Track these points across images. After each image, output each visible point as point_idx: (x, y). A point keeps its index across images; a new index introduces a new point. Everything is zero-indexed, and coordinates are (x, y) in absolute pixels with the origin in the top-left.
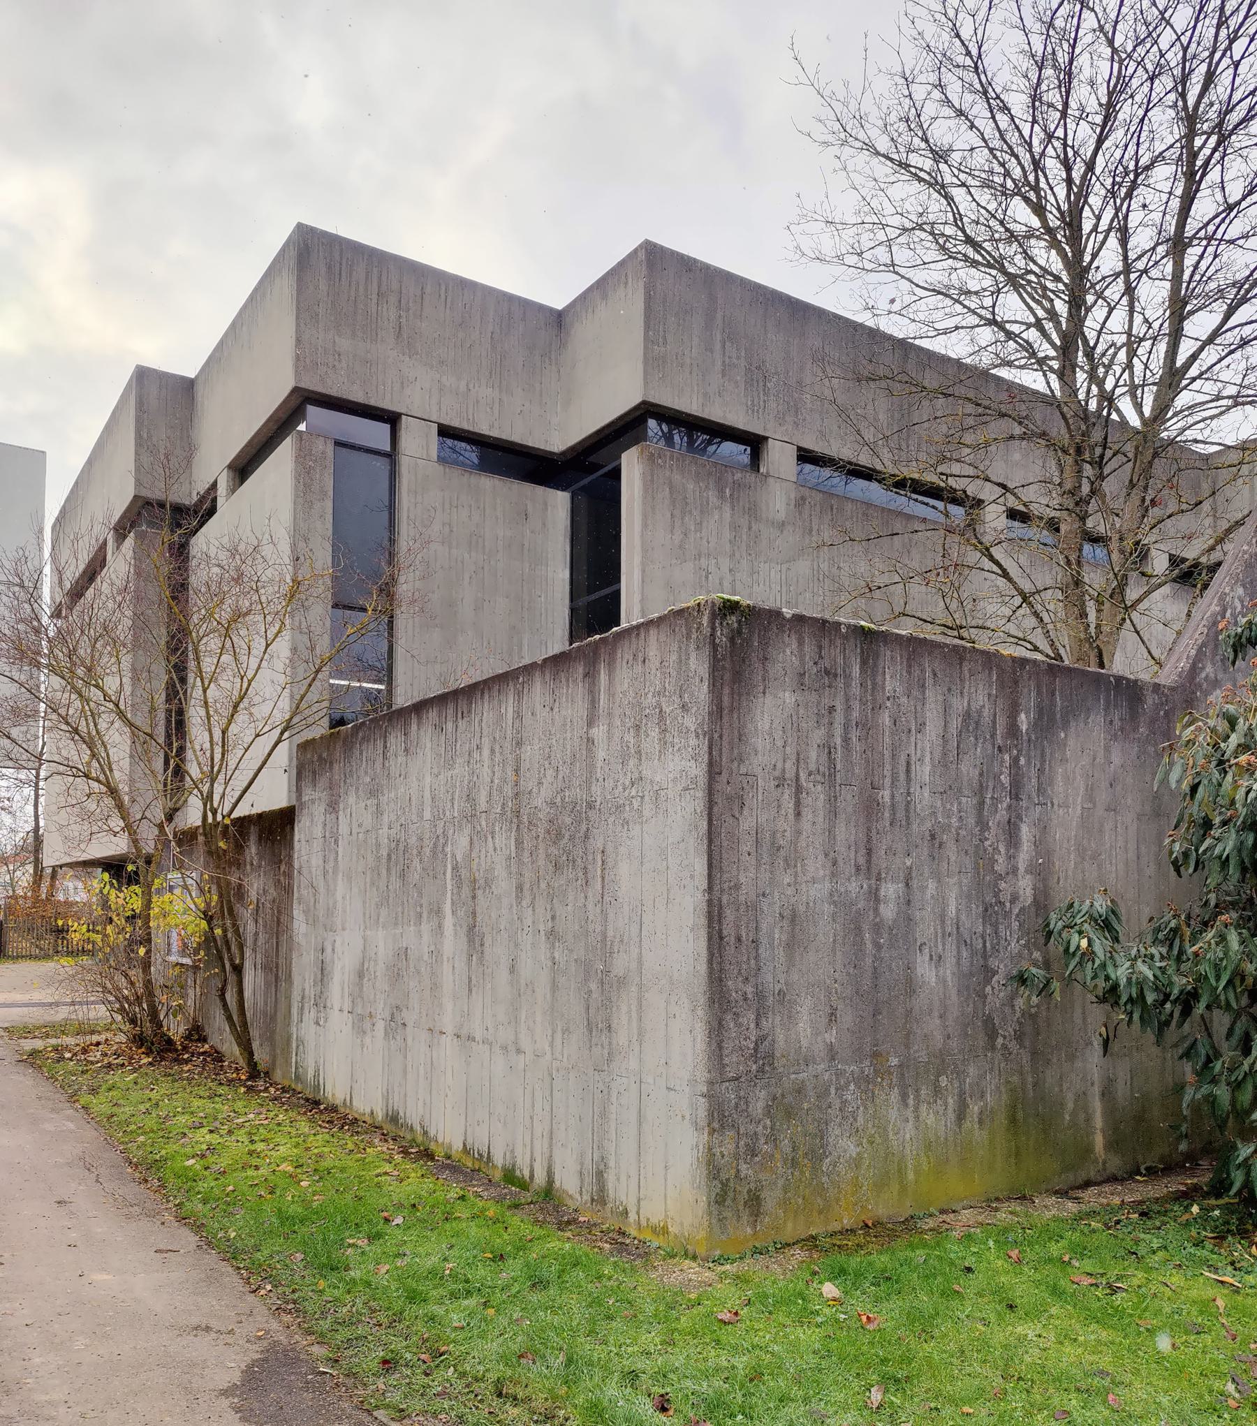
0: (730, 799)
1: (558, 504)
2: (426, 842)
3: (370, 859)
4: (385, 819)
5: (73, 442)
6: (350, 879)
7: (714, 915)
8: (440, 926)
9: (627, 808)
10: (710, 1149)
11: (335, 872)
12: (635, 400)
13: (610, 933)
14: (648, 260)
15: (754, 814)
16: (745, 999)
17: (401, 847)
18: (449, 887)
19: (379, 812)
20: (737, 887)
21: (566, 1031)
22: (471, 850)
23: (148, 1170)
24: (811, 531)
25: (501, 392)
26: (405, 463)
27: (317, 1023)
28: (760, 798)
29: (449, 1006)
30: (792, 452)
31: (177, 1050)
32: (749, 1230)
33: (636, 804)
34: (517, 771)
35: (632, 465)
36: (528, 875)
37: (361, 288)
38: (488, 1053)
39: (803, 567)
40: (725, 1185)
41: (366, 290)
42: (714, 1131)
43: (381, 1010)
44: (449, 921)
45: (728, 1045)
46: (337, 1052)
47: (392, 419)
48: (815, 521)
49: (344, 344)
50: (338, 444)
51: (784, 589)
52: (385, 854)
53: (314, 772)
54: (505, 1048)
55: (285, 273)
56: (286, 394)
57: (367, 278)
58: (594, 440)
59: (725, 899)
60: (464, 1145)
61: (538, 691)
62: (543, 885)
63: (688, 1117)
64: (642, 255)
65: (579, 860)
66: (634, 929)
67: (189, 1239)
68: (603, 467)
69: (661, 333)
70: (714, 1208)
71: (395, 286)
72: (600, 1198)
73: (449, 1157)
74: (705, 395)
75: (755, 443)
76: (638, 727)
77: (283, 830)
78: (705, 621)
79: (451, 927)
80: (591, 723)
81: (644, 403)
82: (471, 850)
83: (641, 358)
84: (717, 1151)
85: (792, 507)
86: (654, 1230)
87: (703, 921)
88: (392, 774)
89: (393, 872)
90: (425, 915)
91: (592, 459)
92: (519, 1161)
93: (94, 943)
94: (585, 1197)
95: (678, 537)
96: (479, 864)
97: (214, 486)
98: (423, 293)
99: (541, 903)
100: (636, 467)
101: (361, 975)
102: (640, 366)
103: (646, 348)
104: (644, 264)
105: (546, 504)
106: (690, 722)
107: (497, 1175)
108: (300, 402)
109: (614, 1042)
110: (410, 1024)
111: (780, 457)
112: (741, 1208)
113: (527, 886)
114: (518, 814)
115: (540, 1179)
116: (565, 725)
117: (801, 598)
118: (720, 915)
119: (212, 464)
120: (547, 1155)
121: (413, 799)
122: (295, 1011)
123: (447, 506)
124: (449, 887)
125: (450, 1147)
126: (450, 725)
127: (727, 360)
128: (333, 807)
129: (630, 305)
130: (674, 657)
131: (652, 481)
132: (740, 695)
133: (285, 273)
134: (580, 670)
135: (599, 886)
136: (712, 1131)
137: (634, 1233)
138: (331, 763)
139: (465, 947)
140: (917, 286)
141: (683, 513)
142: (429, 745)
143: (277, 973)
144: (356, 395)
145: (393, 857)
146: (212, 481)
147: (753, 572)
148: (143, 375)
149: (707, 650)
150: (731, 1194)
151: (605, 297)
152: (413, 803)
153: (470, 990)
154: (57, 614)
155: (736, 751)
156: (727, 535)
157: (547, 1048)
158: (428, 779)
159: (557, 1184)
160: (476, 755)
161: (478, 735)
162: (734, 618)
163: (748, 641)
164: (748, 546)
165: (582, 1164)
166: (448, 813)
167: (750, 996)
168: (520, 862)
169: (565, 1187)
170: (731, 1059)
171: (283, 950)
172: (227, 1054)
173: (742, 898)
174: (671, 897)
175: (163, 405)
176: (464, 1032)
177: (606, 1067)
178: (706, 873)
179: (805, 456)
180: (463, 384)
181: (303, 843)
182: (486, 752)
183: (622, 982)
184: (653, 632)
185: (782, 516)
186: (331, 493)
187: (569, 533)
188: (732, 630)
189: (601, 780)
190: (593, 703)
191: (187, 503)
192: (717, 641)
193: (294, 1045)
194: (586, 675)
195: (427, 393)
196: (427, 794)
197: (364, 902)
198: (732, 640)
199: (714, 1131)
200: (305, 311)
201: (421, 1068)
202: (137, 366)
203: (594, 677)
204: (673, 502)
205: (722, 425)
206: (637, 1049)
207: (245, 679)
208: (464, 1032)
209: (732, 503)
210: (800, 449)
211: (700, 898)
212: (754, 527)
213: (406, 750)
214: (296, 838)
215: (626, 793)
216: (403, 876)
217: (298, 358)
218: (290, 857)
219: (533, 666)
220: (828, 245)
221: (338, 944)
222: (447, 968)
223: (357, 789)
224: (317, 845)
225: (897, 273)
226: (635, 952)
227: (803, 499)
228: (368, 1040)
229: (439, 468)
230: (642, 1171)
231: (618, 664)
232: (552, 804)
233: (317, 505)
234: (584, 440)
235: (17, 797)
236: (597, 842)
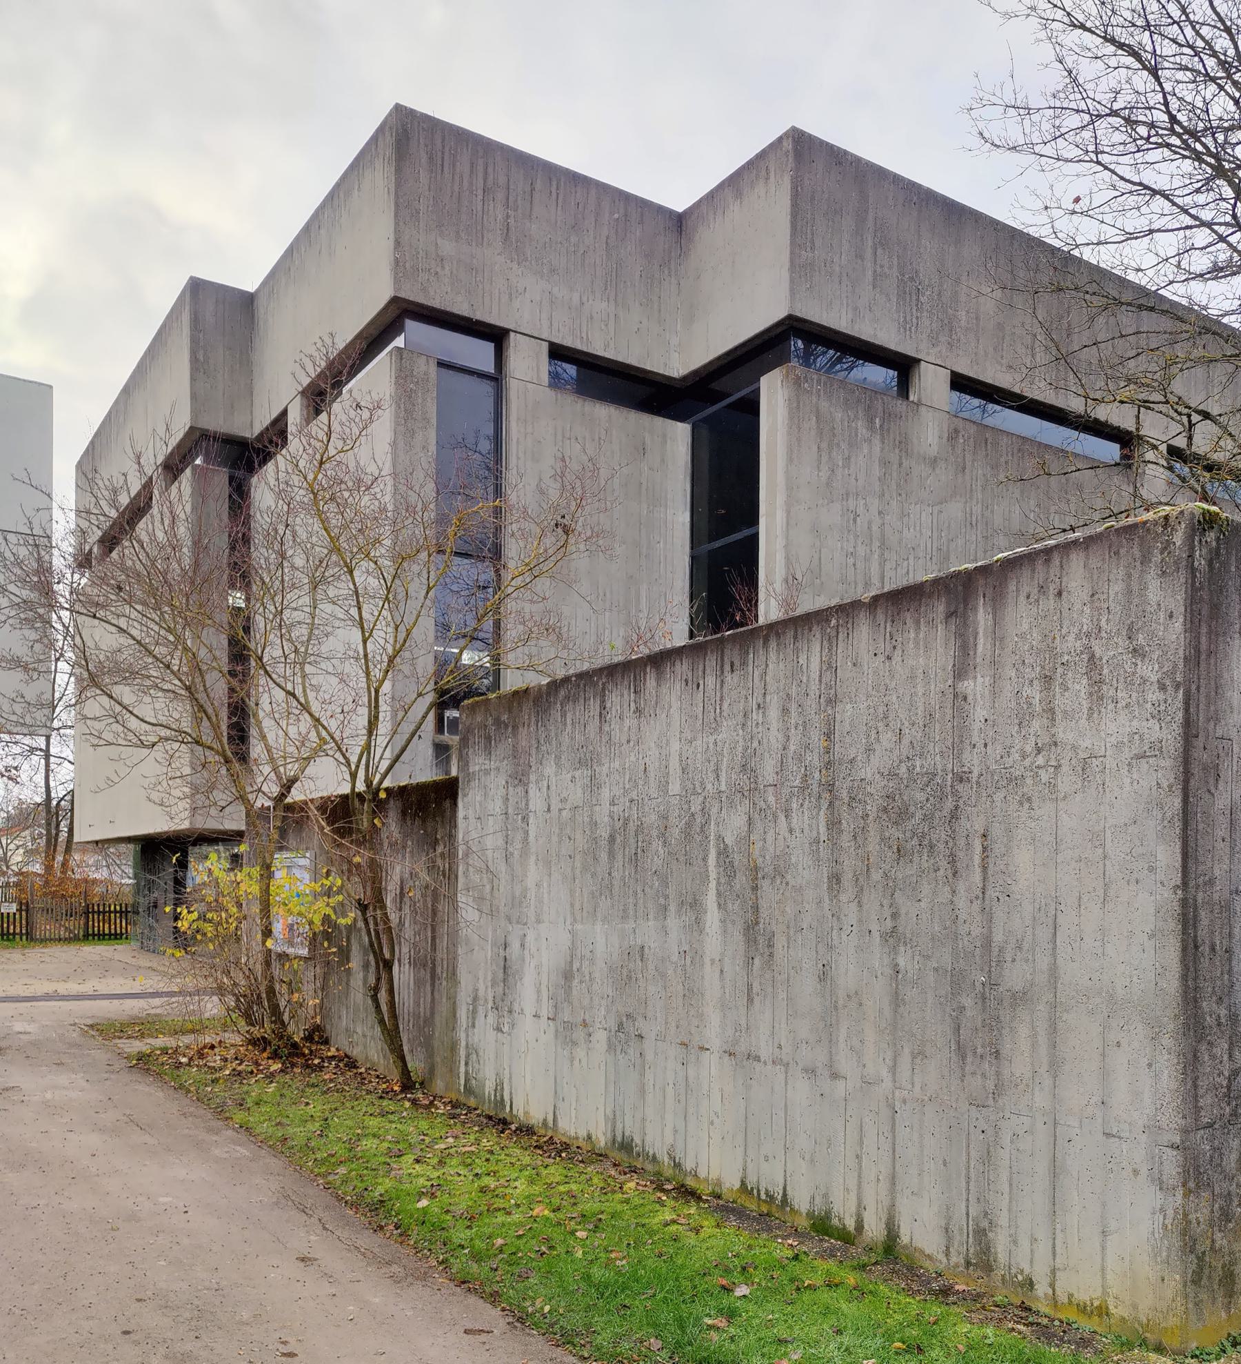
0: (1205, 768)
1: (677, 437)
2: (673, 820)
3: (581, 841)
4: (606, 794)
5: (91, 375)
6: (548, 864)
7: (1188, 918)
8: (698, 921)
9: (1029, 781)
10: (1186, 1215)
11: (525, 853)
12: (779, 314)
13: (998, 937)
14: (795, 150)
15: (1229, 789)
16: (1219, 1024)
17: (632, 826)
18: (713, 875)
19: (594, 785)
20: (1211, 882)
21: (919, 1054)
22: (750, 832)
23: (377, 1212)
24: (964, 468)
25: (616, 304)
26: (514, 388)
27: (499, 1029)
28: (1235, 768)
29: (714, 1018)
30: (945, 376)
31: (304, 1055)
32: (1223, 1314)
33: (1044, 776)
34: (829, 735)
35: (774, 391)
36: (849, 864)
37: (466, 184)
38: (782, 1077)
39: (955, 509)
40: (1200, 1259)
41: (471, 184)
42: (1190, 1191)
43: (603, 1020)
44: (712, 916)
45: (1203, 1083)
46: (524, 1060)
47: (497, 336)
48: (969, 457)
49: (447, 247)
50: (441, 364)
51: (935, 534)
52: (605, 835)
53: (488, 739)
54: (811, 1071)
55: (378, 164)
56: (382, 306)
57: (472, 172)
58: (715, 367)
59: (1200, 896)
60: (743, 1183)
61: (863, 637)
62: (876, 876)
63: (1144, 1171)
64: (788, 145)
65: (941, 846)
66: (1044, 934)
67: (492, 1316)
68: (729, 395)
69: (809, 236)
70: (1190, 1289)
71: (502, 180)
72: (983, 1261)
73: (719, 1197)
74: (856, 309)
75: (904, 366)
76: (1048, 679)
77: (439, 804)
78: (1179, 538)
79: (717, 923)
80: (960, 672)
81: (790, 318)
82: (750, 832)
83: (787, 265)
84: (1192, 1217)
85: (945, 440)
86: (1082, 1309)
87: (1173, 925)
88: (616, 739)
89: (619, 857)
90: (673, 908)
91: (715, 386)
92: (837, 1208)
93: (204, 934)
94: (954, 1260)
95: (824, 474)
96: (763, 848)
97: (284, 413)
98: (533, 190)
99: (873, 899)
100: (780, 391)
101: (568, 976)
102: (785, 274)
103: (792, 253)
104: (791, 155)
105: (664, 436)
106: (1150, 671)
107: (803, 1223)
108: (399, 314)
109: (1006, 1072)
110: (650, 1036)
111: (932, 384)
112: (1216, 1287)
113: (847, 878)
114: (830, 787)
115: (874, 1230)
116: (913, 677)
117: (953, 545)
118: (1195, 917)
119: (279, 388)
120: (887, 1203)
121: (651, 769)
122: (462, 1014)
123: (559, 437)
124: (713, 875)
125: (719, 1183)
126: (711, 681)
127: (879, 270)
128: (520, 778)
129: (773, 204)
130: (1117, 587)
131: (798, 407)
132: (1217, 635)
133: (378, 164)
134: (941, 608)
135: (977, 877)
136: (1188, 1193)
137: (1044, 1308)
138: (515, 728)
139: (742, 947)
140: (1122, 178)
141: (830, 447)
142: (676, 705)
143: (436, 970)
144: (460, 307)
145: (619, 839)
146: (275, 415)
147: (903, 515)
148: (196, 288)
149: (1182, 576)
150: (1206, 1271)
151: (739, 195)
152: (652, 775)
153: (750, 1000)
154: (83, 561)
155: (1212, 708)
156: (877, 471)
157: (884, 1073)
158: (675, 746)
159: (905, 1239)
160: (756, 716)
161: (758, 692)
162: (1212, 534)
163: (1226, 565)
164: (898, 485)
165: (949, 1219)
166: (709, 787)
167: (1223, 1020)
168: (834, 845)
169: (918, 1243)
170: (1206, 1100)
171: (443, 943)
172: (361, 1059)
173: (1216, 896)
174: (1112, 893)
175: (218, 321)
176: (742, 1048)
177: (991, 1102)
178: (1178, 864)
179: (961, 383)
180: (576, 297)
181: (472, 820)
182: (774, 713)
183: (1019, 998)
184: (1076, 560)
185: (933, 451)
186: (434, 421)
187: (689, 471)
188: (1210, 551)
189: (980, 745)
190: (965, 649)
191: (248, 435)
192: (1196, 564)
193: (463, 1053)
194: (949, 615)
195: (540, 306)
196: (674, 764)
197: (572, 892)
198: (1210, 563)
199: (1190, 1191)
200: (404, 209)
201: (670, 1090)
202: (191, 278)
203: (965, 617)
204: (820, 433)
205: (873, 345)
206: (1048, 1082)
207: (402, 628)
208: (742, 1048)
209: (882, 435)
210: (953, 372)
211: (1169, 898)
212: (905, 463)
213: (637, 710)
214: (461, 813)
215: (1027, 762)
216: (635, 860)
217: (397, 261)
218: (452, 837)
219: (856, 605)
220: (1013, 131)
221: (530, 938)
222: (710, 975)
223: (558, 758)
224: (492, 824)
225: (1098, 163)
226: (1043, 962)
227: (956, 431)
228: (580, 1052)
229: (550, 393)
230: (1059, 1236)
231: (1010, 599)
232: (892, 775)
233: (419, 437)
234: (711, 363)
235: (26, 766)
236: (974, 823)
